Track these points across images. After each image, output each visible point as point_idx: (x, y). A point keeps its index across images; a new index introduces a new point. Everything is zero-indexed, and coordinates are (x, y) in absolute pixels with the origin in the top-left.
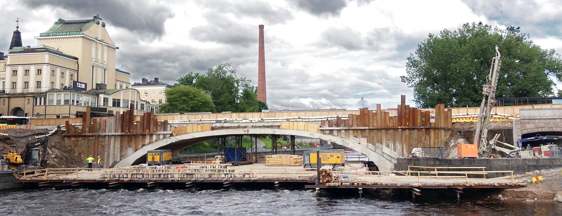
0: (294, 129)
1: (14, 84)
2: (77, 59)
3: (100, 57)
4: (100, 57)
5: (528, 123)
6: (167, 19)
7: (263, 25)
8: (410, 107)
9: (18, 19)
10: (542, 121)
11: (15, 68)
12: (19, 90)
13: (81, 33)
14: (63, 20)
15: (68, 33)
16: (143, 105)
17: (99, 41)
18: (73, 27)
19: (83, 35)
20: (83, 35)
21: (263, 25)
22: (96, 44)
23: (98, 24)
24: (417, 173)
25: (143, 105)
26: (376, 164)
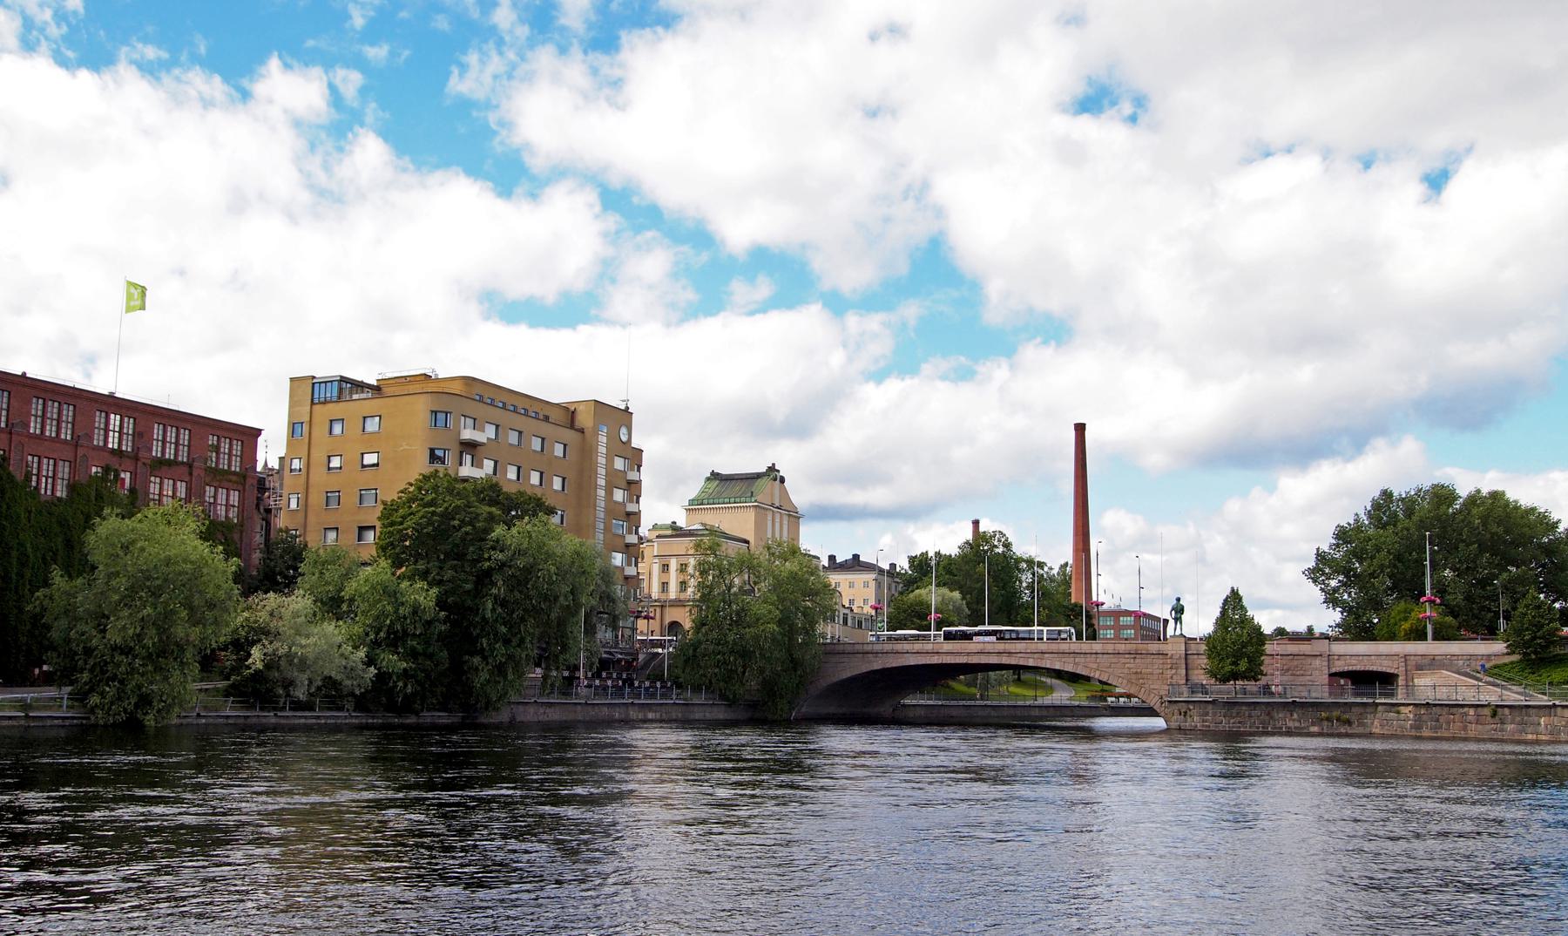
0: (444, 414)
1: (664, 586)
2: (747, 542)
3: (777, 535)
4: (777, 535)
5: (1338, 659)
6: (1215, 632)
7: (1085, 424)
8: (861, 559)
9: (137, 296)
10: (1353, 658)
11: (665, 561)
12: (673, 593)
13: (753, 500)
14: (718, 474)
15: (732, 500)
16: (847, 614)
17: (777, 508)
18: (738, 487)
19: (756, 504)
20: (756, 504)
21: (1085, 424)
22: (773, 515)
23: (775, 480)
24: (1042, 631)
25: (847, 614)
26: (1217, 613)
